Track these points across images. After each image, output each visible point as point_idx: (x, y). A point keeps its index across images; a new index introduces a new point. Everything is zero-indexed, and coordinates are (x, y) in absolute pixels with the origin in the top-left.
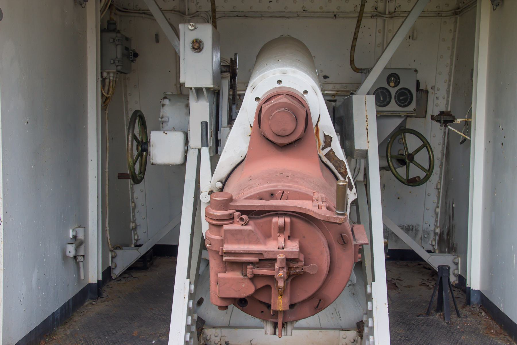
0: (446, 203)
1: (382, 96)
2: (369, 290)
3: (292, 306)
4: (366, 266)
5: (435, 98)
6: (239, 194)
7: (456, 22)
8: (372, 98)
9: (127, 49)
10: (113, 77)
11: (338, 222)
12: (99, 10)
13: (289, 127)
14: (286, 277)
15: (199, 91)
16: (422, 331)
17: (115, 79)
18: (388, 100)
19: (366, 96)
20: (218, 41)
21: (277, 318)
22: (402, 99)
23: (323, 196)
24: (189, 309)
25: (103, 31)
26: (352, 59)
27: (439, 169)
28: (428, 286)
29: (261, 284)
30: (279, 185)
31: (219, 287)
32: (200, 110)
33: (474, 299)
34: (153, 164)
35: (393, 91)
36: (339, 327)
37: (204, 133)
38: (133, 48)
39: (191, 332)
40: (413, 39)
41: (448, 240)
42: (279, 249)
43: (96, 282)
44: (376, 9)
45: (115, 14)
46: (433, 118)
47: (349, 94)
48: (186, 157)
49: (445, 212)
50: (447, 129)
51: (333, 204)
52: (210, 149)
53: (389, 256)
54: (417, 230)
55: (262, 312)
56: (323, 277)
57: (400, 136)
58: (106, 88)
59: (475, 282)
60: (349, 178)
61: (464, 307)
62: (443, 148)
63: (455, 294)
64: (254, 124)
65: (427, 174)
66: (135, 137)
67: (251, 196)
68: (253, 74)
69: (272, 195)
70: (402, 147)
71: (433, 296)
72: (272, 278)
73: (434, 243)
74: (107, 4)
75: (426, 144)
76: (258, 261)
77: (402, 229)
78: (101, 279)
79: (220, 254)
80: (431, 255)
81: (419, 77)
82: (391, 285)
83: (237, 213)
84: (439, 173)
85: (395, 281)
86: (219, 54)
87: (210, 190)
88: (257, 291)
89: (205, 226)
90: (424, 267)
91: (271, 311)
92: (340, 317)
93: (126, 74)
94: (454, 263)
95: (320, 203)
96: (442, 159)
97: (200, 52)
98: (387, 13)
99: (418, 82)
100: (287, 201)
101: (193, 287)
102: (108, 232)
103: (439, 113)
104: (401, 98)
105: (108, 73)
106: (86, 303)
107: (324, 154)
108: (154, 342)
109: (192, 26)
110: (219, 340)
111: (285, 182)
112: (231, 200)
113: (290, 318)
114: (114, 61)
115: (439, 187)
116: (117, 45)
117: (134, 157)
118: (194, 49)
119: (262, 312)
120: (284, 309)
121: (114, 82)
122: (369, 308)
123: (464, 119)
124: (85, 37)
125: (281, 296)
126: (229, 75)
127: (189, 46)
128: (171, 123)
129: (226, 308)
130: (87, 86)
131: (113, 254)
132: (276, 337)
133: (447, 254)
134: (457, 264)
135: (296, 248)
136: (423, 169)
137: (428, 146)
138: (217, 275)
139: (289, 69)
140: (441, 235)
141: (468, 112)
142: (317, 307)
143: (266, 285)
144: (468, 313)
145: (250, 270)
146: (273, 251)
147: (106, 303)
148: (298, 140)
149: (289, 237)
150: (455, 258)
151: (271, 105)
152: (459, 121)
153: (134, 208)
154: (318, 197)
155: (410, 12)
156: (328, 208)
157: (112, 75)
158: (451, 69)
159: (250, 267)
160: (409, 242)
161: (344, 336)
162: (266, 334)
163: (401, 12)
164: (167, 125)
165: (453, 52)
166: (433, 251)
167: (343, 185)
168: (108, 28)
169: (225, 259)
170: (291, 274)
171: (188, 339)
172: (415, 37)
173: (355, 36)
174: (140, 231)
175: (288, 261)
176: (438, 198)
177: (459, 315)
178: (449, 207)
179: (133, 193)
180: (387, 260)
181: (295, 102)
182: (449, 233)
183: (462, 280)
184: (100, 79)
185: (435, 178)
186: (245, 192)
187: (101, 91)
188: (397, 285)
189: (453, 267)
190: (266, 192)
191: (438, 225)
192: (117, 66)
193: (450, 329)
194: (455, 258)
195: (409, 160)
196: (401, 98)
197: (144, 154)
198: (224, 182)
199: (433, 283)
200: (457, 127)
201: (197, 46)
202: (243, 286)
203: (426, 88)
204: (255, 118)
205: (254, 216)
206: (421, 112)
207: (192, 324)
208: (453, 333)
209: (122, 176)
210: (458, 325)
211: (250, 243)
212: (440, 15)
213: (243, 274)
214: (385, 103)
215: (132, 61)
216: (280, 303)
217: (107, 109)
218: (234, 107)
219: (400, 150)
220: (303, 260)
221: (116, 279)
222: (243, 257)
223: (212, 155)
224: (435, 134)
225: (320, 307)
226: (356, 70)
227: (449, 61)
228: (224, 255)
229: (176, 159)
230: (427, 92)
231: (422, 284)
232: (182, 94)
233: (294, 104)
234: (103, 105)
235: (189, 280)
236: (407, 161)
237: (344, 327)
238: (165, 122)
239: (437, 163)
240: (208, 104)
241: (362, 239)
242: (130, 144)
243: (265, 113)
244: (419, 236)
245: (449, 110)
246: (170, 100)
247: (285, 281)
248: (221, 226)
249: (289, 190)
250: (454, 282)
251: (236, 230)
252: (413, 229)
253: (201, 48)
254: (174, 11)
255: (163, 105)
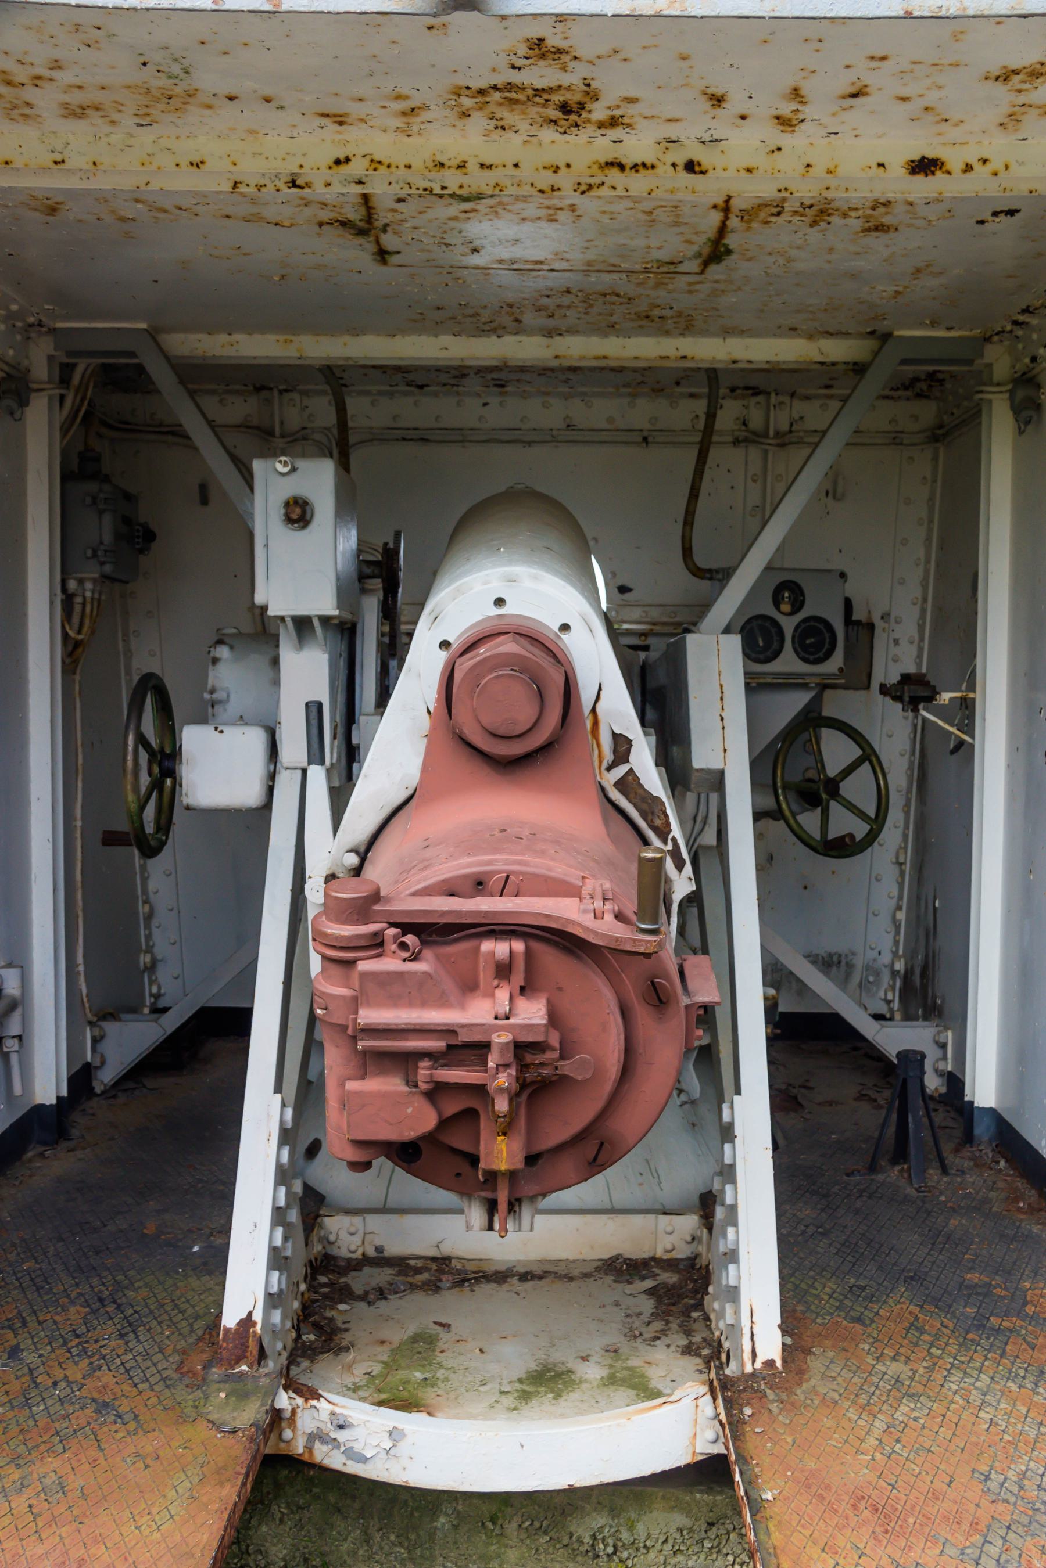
0: (919, 898)
1: (758, 637)
2: (726, 1117)
3: (531, 1160)
4: (722, 1056)
5: (891, 641)
6: (396, 882)
7: (935, 459)
8: (734, 643)
9: (127, 521)
10: (93, 592)
11: (642, 950)
12: (57, 426)
13: (523, 713)
14: (515, 1087)
15: (303, 625)
16: (857, 1212)
17: (96, 596)
18: (775, 645)
19: (721, 636)
20: (349, 502)
21: (494, 1190)
22: (811, 645)
23: (607, 885)
24: (279, 1167)
25: (66, 477)
26: (687, 546)
27: (901, 816)
28: (875, 1100)
29: (452, 1107)
30: (497, 861)
31: (349, 1115)
32: (306, 674)
33: (982, 1129)
34: (188, 808)
35: (789, 625)
36: (658, 1206)
37: (315, 731)
38: (142, 520)
39: (287, 1226)
40: (834, 497)
41: (924, 987)
42: (496, 1018)
43: (54, 1101)
44: (745, 424)
45: (100, 436)
46: (884, 690)
47: (679, 630)
48: (270, 790)
49: (916, 920)
50: (920, 718)
51: (630, 908)
52: (328, 771)
53: (778, 1031)
54: (850, 966)
55: (458, 1175)
56: (608, 1087)
57: (805, 736)
58: (76, 619)
59: (984, 1090)
60: (674, 839)
61: (957, 1150)
62: (911, 763)
63: (939, 1118)
64: (435, 708)
65: (871, 829)
66: (142, 740)
67: (426, 888)
68: (434, 586)
69: (479, 885)
70: (810, 761)
71: (884, 1126)
72: (480, 1090)
73: (890, 997)
74: (78, 411)
75: (869, 755)
76: (444, 1049)
77: (814, 963)
78: (64, 1093)
79: (350, 1032)
80: (883, 1027)
81: (850, 589)
82: (783, 1101)
83: (392, 932)
84: (902, 824)
85: (795, 1091)
86: (354, 533)
87: (329, 872)
88: (444, 1123)
89: (316, 964)
90: (867, 1056)
91: (480, 1173)
92: (660, 1183)
93: (127, 583)
94: (937, 1043)
95: (598, 904)
96: (909, 791)
97: (304, 527)
98: (771, 433)
99: (848, 604)
100: (518, 901)
101: (289, 1113)
102: (82, 978)
103: (899, 678)
104: (808, 642)
105: (81, 582)
106: (30, 1154)
107: (613, 782)
108: (196, 1249)
109: (285, 464)
110: (359, 1243)
111: (511, 853)
112: (376, 897)
113: (527, 1189)
114: (95, 552)
115: (901, 860)
116: (101, 513)
117: (143, 789)
118: (289, 520)
119: (458, 1175)
120: (512, 1168)
121: (96, 604)
122: (728, 1160)
123: (958, 695)
124: (22, 494)
125: (504, 1134)
126: (381, 586)
127: (277, 514)
128: (233, 708)
129: (366, 1166)
130: (25, 615)
131: (97, 1032)
132: (494, 1235)
133: (920, 1023)
134: (943, 1046)
135: (541, 1017)
136: (862, 815)
137: (874, 759)
138: (343, 1085)
139: (520, 570)
140: (907, 977)
141: (968, 675)
142: (595, 1159)
143: (464, 1110)
144: (968, 1164)
145: (424, 1071)
146: (483, 1025)
147: (80, 1154)
148: (546, 749)
149: (522, 989)
150: (939, 1033)
151: (478, 659)
152: (946, 697)
153: (149, 917)
154: (594, 889)
155: (824, 433)
156: (619, 916)
157: (89, 585)
158: (927, 572)
159: (425, 1063)
160: (830, 994)
161: (669, 1229)
162: (469, 1228)
163: (806, 431)
164: (225, 710)
165: (930, 530)
166: (888, 1016)
167: (654, 860)
168: (78, 472)
169: (361, 1045)
170: (528, 1080)
171: (278, 1242)
172: (840, 490)
173: (692, 488)
174: (164, 974)
175: (521, 1049)
176: (901, 885)
177: (945, 1170)
178: (926, 907)
179: (145, 880)
180: (771, 1040)
181: (537, 651)
182: (928, 970)
183: (955, 1082)
184: (59, 597)
185: (892, 835)
186: (405, 881)
187: (63, 627)
188: (800, 1100)
189: (932, 1055)
190: (465, 877)
191: (901, 952)
192: (102, 564)
193: (924, 1202)
194: (939, 1033)
195: (827, 793)
196: (808, 642)
197: (169, 781)
198: (365, 852)
199: (887, 1093)
200: (942, 712)
201: (298, 513)
202: (410, 1110)
203: (870, 617)
204: (439, 693)
205: (434, 938)
206: (857, 674)
207: (288, 1205)
208: (929, 1213)
209: (111, 839)
210: (941, 1193)
211: (424, 1004)
212: (898, 441)
213: (407, 1083)
214: (769, 653)
215: (141, 551)
216: (501, 1151)
217: (78, 671)
218: (393, 664)
219: (807, 769)
220: (557, 1045)
221: (103, 1093)
222: (407, 1040)
223: (336, 784)
224: (892, 731)
225: (599, 1161)
226: (698, 572)
227: (921, 553)
228: (359, 1036)
229: (246, 793)
230: (871, 627)
231: (861, 1097)
232: (262, 633)
233: (536, 658)
234: (68, 661)
235: (278, 1096)
236: (824, 796)
237: (669, 1206)
238: (220, 702)
239: (896, 801)
240: (326, 657)
241: (705, 990)
242: (130, 757)
243: (463, 679)
244: (856, 979)
245: (924, 671)
246: (232, 647)
247: (513, 1098)
248: (351, 963)
249: (521, 873)
250: (936, 1089)
251: (389, 974)
252: (839, 962)
253: (308, 517)
254: (245, 426)
255: (215, 661)
